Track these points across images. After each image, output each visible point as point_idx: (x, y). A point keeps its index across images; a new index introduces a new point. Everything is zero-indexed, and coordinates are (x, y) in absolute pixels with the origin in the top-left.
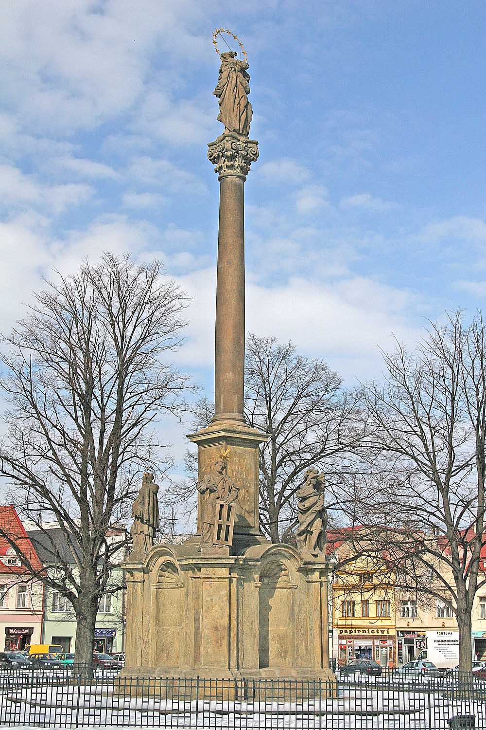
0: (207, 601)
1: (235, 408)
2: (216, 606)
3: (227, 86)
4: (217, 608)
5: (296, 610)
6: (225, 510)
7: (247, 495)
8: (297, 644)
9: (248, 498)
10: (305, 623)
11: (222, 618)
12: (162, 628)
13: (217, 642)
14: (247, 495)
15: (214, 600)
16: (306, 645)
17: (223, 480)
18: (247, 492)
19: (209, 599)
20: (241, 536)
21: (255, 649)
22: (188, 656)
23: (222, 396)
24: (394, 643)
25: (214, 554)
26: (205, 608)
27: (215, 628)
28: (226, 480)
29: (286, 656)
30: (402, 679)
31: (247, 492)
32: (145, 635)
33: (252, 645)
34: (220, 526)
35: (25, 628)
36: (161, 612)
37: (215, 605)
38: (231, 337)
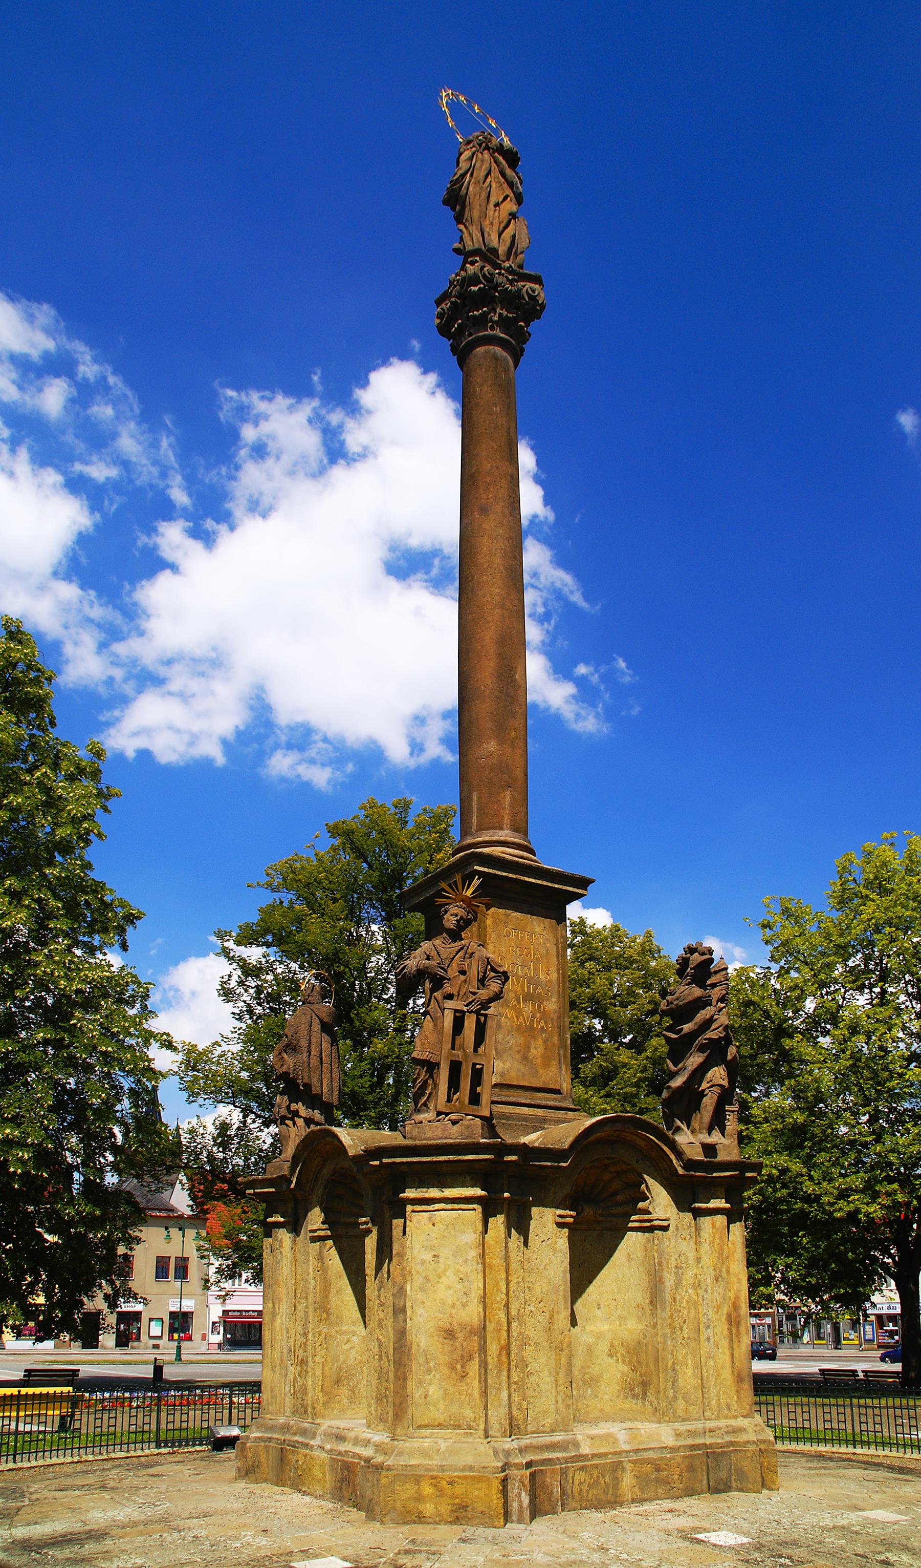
0: (423, 1263)
1: (507, 820)
2: (447, 1273)
3: (472, 175)
4: (450, 1278)
5: (669, 1280)
6: (470, 1023)
7: (538, 1015)
8: (673, 1363)
9: (542, 1024)
10: (693, 1311)
11: (464, 1305)
12: (338, 1329)
13: (454, 1368)
14: (538, 1015)
15: (441, 1260)
16: (699, 1366)
17: (461, 954)
18: (539, 1008)
19: (428, 1256)
20: (525, 1110)
21: (560, 1382)
22: (385, 1401)
23: (475, 797)
24: (773, 1320)
25: (446, 1138)
26: (418, 1280)
27: (447, 1331)
28: (470, 951)
29: (644, 1394)
30: (902, 1426)
31: (539, 1008)
32: (301, 1346)
33: (553, 1373)
34: (455, 1068)
35: (254, 1311)
36: (333, 1291)
37: (445, 1271)
38: (492, 664)
